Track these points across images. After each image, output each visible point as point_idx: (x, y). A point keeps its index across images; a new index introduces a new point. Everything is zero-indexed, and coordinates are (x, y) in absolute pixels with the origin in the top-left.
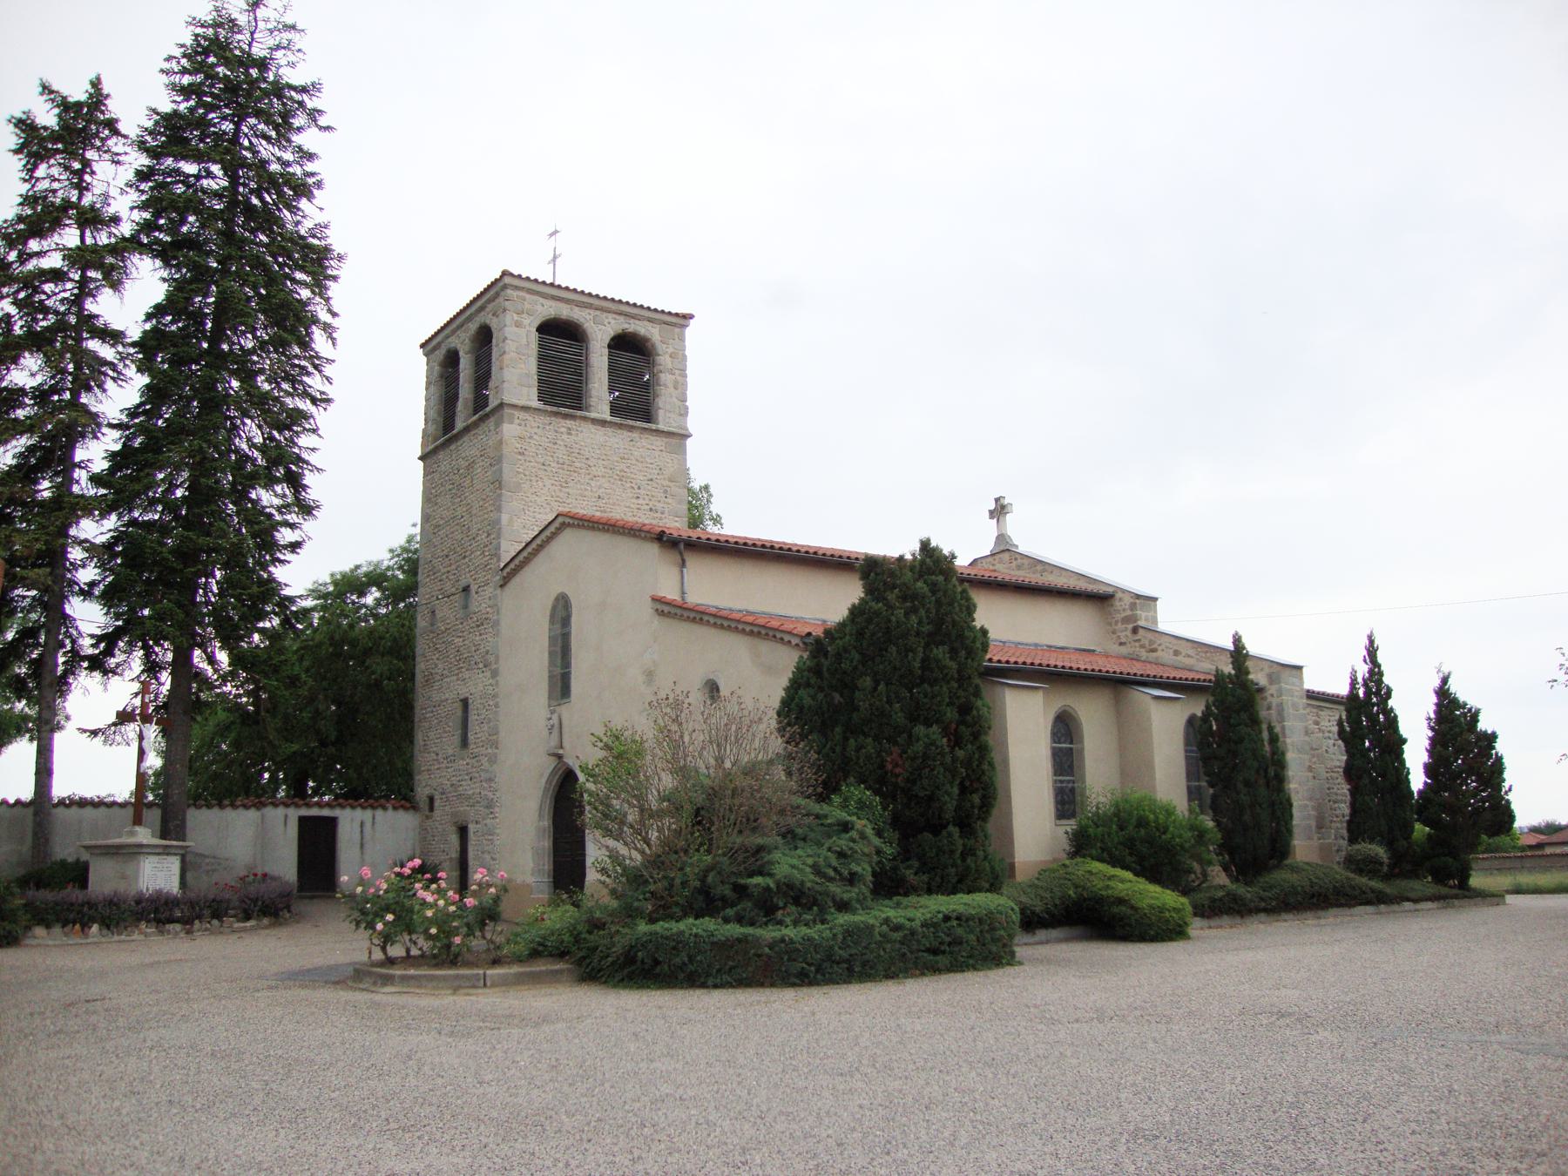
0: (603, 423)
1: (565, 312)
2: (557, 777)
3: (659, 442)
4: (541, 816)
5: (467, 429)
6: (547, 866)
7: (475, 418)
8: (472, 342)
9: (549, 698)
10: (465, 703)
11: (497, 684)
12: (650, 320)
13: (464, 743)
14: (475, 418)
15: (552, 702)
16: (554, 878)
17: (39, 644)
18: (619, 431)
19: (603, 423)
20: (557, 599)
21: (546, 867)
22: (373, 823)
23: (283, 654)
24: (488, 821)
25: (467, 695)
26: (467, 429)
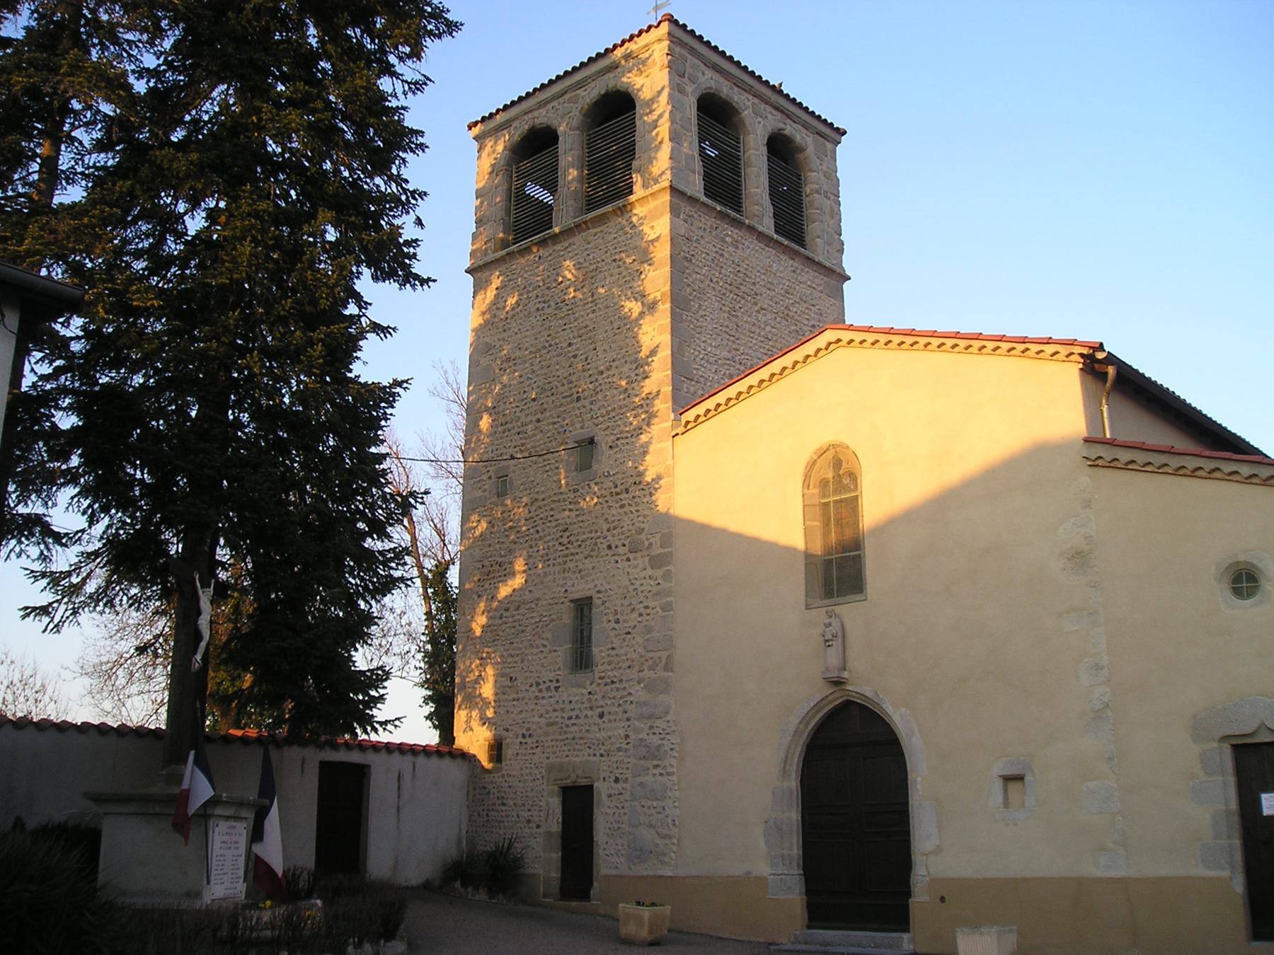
0: (761, 236)
1: (726, 90)
2: (821, 715)
3: (810, 275)
4: (784, 772)
5: (568, 232)
6: (794, 847)
7: (504, 252)
8: (585, 115)
9: (806, 596)
10: (583, 607)
11: (667, 577)
12: (805, 126)
13: (582, 659)
14: (504, 252)
15: (810, 601)
16: (805, 868)
17: (146, 303)
18: (783, 257)
19: (761, 236)
20: (822, 452)
21: (795, 851)
22: (414, 776)
23: (828, 482)
24: (648, 779)
25: (592, 593)
26: (568, 232)
